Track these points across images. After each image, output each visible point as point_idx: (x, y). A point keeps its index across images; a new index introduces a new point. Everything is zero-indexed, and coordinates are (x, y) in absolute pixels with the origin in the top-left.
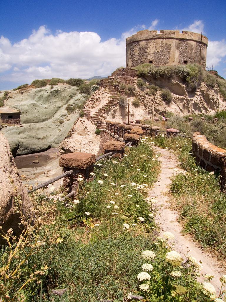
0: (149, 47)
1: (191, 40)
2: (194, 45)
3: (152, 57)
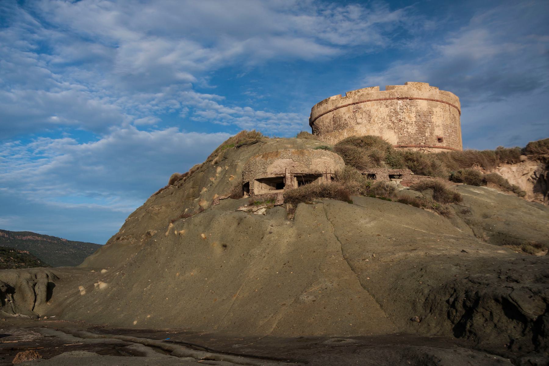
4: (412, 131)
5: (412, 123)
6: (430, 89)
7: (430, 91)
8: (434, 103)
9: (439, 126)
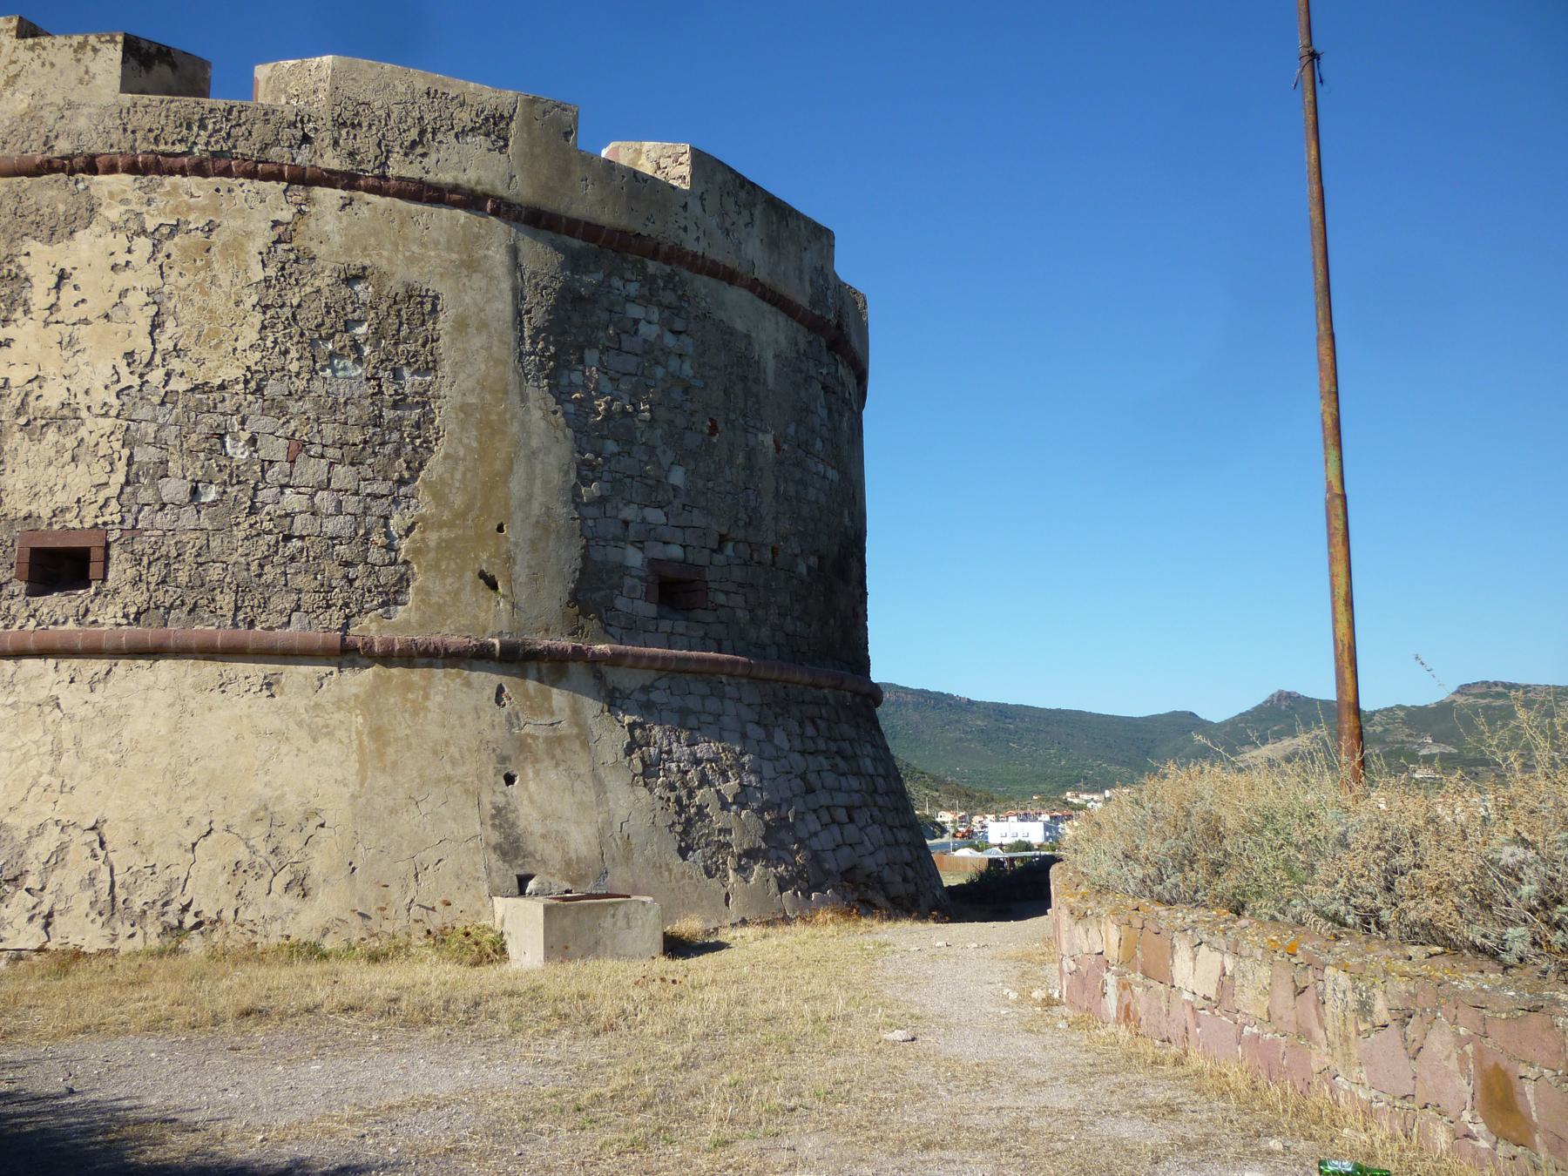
0: (39, 296)
1: (729, 276)
2: (770, 364)
3: (79, 480)
6: (13, 70)
7: (20, 82)
8: (50, 193)
9: (64, 419)
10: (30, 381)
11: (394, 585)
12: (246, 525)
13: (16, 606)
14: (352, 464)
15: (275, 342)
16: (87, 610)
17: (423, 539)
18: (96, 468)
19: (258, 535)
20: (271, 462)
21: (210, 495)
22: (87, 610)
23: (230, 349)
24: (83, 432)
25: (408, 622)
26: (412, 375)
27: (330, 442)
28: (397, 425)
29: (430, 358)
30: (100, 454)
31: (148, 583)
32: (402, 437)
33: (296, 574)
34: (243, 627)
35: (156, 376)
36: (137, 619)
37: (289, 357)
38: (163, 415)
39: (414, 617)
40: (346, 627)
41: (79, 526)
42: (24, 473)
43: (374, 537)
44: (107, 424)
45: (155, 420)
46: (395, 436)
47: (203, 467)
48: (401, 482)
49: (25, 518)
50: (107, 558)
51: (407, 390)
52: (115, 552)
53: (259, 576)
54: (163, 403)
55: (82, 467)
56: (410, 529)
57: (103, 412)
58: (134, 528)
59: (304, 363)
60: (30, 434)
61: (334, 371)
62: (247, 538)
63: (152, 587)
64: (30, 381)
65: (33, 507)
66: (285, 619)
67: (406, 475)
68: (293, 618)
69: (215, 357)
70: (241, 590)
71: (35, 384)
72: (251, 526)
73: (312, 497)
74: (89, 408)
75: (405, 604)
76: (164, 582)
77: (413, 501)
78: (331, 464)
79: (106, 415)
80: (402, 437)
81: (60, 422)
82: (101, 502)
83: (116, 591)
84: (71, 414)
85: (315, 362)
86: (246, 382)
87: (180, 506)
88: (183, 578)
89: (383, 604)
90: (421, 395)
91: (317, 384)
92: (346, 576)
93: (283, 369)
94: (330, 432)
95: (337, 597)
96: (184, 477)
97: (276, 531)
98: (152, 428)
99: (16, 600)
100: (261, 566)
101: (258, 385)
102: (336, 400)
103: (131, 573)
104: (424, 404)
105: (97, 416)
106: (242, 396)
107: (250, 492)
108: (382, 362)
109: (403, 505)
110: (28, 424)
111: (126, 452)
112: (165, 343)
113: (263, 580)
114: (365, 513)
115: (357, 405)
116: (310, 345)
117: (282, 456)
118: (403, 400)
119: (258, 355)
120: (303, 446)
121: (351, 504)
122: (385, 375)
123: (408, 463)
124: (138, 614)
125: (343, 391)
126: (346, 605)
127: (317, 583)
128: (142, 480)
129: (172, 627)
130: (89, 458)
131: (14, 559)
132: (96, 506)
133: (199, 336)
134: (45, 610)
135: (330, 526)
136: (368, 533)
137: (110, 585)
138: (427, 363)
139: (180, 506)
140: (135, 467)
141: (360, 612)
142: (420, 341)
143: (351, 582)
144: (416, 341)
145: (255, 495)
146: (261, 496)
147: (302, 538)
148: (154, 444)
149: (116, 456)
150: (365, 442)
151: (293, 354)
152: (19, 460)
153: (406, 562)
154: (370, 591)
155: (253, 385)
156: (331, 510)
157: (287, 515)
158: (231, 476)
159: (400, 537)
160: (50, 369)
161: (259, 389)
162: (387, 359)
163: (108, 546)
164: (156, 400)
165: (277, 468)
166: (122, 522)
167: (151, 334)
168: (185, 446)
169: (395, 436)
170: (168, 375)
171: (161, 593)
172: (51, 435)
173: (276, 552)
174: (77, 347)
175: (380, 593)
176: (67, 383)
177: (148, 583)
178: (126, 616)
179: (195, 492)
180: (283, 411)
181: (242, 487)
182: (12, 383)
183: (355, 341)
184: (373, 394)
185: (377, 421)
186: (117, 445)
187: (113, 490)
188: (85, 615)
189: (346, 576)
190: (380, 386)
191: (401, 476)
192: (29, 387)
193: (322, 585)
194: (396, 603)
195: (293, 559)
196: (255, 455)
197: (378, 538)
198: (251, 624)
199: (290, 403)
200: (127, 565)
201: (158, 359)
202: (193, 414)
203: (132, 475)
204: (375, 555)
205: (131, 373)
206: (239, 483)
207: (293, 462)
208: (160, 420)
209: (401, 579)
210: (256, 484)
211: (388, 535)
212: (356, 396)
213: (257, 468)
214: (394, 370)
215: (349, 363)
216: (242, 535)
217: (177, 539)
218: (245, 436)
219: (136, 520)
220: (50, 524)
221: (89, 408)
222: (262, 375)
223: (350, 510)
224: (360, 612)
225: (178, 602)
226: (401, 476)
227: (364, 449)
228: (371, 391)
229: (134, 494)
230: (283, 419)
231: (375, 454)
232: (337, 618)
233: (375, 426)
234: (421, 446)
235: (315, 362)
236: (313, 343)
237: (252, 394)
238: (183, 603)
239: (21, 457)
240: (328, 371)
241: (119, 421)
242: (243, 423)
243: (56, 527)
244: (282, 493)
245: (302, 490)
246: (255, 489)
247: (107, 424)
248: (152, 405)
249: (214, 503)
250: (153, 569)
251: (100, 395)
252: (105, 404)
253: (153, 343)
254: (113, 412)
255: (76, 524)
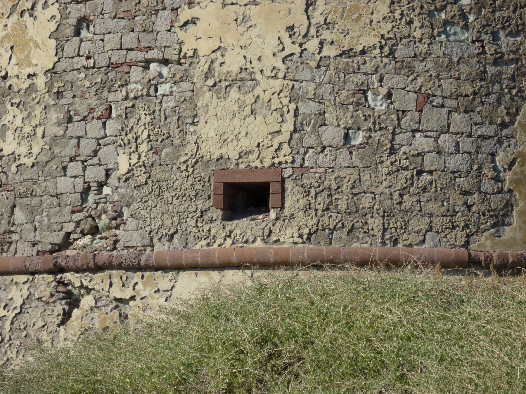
4: (23, 150)
5: (32, 88)
10: (214, 52)
11: (502, 210)
12: (388, 163)
13: (215, 228)
14: (466, 112)
15: (402, 14)
16: (271, 232)
17: (522, 172)
18: (270, 119)
19: (398, 171)
20: (404, 112)
21: (359, 138)
22: (271, 232)
23: (368, 21)
24: (258, 91)
25: (514, 239)
26: (506, 36)
27: (448, 94)
28: (497, 78)
29: (519, 22)
30: (273, 108)
31: (316, 210)
32: (502, 89)
33: (428, 201)
34: (389, 245)
35: (312, 45)
36: (309, 239)
37: (413, 26)
38: (320, 76)
39: (519, 236)
40: (467, 244)
41: (260, 165)
42: (214, 124)
43: (485, 171)
44: (277, 84)
45: (313, 80)
46: (497, 87)
47: (352, 117)
48: (503, 125)
49: (218, 160)
50: (283, 190)
51: (504, 49)
52: (289, 185)
53: (400, 203)
54: (318, 67)
55: (259, 118)
56: (512, 164)
57: (273, 74)
58: (302, 166)
59: (425, 30)
60: (218, 93)
61: (448, 36)
62: (389, 174)
63: (319, 213)
64: (214, 52)
65: (224, 151)
66: (421, 238)
67: (507, 119)
68: (427, 237)
69: (356, 28)
70: (387, 215)
71: (219, 53)
72: (392, 163)
73: (437, 139)
74: (262, 71)
75: (510, 225)
76: (328, 209)
77: (513, 141)
78: (450, 112)
79: (275, 77)
80: (502, 89)
81: (240, 83)
82: (276, 146)
83: (292, 217)
84: (248, 77)
85: (433, 29)
86: (382, 47)
87: (337, 148)
88: (342, 206)
89: (493, 227)
90: (514, 52)
91: (436, 47)
92: (465, 203)
93: (409, 36)
94: (449, 87)
95: (460, 219)
96: (339, 126)
97: (411, 167)
98: (311, 87)
99: (215, 224)
100: (401, 196)
101: (390, 49)
102: (451, 61)
103: (303, 202)
104: (517, 60)
105: (268, 78)
106: (379, 59)
107: (390, 136)
108: (484, 26)
109: (505, 144)
110: (215, 85)
111: (292, 106)
112: (317, 18)
113: (403, 207)
114: (477, 152)
115: (466, 63)
116: (429, 15)
117: (412, 106)
118: (501, 57)
119: (389, 25)
120: (428, 97)
121: (466, 144)
122: (486, 37)
123: (507, 109)
124: (310, 234)
125: (456, 52)
126: (467, 226)
127: (444, 209)
128: (306, 128)
129: (336, 245)
130: (264, 111)
131: (211, 192)
132: (272, 149)
133: (344, 11)
134: (238, 232)
135: (452, 163)
136: (480, 168)
137: (287, 211)
138: (518, 26)
139: (337, 148)
140: (300, 118)
141: (477, 232)
142: (511, 8)
143: (469, 207)
144: (508, 8)
145: (393, 139)
146: (399, 138)
147: (430, 172)
148: (313, 100)
149: (285, 109)
150: (475, 93)
151: (417, 23)
152: (210, 114)
153: (510, 191)
154: (484, 215)
155: (386, 49)
156: (452, 149)
157: (419, 154)
158: (374, 123)
159: (505, 170)
160: (229, 41)
161: (392, 53)
162: (488, 25)
163: (283, 181)
164: (314, 64)
165: (408, 117)
166: (293, 162)
167: (306, 11)
168: (338, 100)
169: (497, 87)
170: (321, 43)
171: (326, 218)
172: (234, 93)
173: (412, 184)
174: (249, 24)
175: (491, 216)
176: (243, 52)
177: (316, 210)
178: (301, 236)
179: (347, 137)
180: (411, 70)
181: (383, 132)
182: (200, 53)
183: (462, 10)
184: (479, 54)
185: (482, 76)
186: (286, 101)
187: (285, 137)
188: (269, 236)
189: (465, 203)
190: (483, 47)
191: (503, 121)
192: (214, 56)
193: (448, 210)
194: (504, 224)
195: (424, 189)
196: (392, 107)
197: (487, 171)
198: (396, 242)
199: (416, 64)
200: (299, 196)
201: (313, 31)
202: (342, 75)
203: (298, 125)
204: (487, 186)
205: (293, 43)
206: (381, 129)
207: (421, 111)
208: (317, 80)
209: (507, 204)
210: (394, 130)
211: (495, 169)
212: (466, 56)
213: (394, 117)
214: (492, 33)
215: (458, 29)
216: (385, 171)
217: (336, 174)
218: (384, 91)
219: (303, 159)
220: (237, 164)
221: (262, 71)
222: (393, 42)
223: (466, 149)
224: (477, 232)
225: (340, 225)
226: (503, 121)
227: (474, 99)
228: (477, 51)
229: (301, 139)
230: (412, 77)
231: (482, 103)
232: (460, 235)
233: (481, 80)
234: (516, 95)
235: (433, 29)
236: (431, 14)
237: (387, 57)
238: (343, 226)
239: (212, 111)
240: (443, 36)
241: (286, 82)
242: (381, 80)
243: (242, 166)
244: (414, 136)
245: (429, 133)
246: (394, 134)
247: (277, 84)
248: (311, 68)
249: (361, 146)
250: (319, 199)
251: (270, 62)
252: (274, 68)
253: (308, 18)
254: (281, 75)
255: (257, 164)
